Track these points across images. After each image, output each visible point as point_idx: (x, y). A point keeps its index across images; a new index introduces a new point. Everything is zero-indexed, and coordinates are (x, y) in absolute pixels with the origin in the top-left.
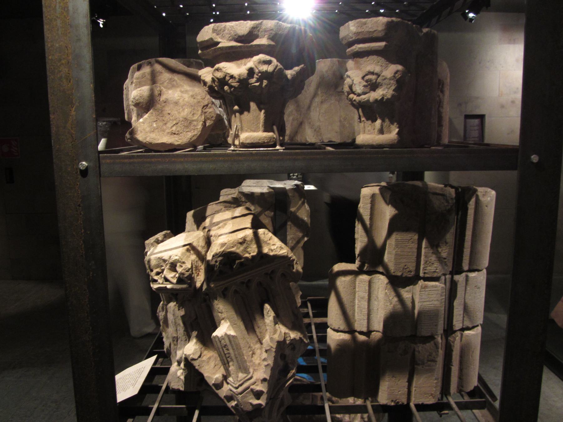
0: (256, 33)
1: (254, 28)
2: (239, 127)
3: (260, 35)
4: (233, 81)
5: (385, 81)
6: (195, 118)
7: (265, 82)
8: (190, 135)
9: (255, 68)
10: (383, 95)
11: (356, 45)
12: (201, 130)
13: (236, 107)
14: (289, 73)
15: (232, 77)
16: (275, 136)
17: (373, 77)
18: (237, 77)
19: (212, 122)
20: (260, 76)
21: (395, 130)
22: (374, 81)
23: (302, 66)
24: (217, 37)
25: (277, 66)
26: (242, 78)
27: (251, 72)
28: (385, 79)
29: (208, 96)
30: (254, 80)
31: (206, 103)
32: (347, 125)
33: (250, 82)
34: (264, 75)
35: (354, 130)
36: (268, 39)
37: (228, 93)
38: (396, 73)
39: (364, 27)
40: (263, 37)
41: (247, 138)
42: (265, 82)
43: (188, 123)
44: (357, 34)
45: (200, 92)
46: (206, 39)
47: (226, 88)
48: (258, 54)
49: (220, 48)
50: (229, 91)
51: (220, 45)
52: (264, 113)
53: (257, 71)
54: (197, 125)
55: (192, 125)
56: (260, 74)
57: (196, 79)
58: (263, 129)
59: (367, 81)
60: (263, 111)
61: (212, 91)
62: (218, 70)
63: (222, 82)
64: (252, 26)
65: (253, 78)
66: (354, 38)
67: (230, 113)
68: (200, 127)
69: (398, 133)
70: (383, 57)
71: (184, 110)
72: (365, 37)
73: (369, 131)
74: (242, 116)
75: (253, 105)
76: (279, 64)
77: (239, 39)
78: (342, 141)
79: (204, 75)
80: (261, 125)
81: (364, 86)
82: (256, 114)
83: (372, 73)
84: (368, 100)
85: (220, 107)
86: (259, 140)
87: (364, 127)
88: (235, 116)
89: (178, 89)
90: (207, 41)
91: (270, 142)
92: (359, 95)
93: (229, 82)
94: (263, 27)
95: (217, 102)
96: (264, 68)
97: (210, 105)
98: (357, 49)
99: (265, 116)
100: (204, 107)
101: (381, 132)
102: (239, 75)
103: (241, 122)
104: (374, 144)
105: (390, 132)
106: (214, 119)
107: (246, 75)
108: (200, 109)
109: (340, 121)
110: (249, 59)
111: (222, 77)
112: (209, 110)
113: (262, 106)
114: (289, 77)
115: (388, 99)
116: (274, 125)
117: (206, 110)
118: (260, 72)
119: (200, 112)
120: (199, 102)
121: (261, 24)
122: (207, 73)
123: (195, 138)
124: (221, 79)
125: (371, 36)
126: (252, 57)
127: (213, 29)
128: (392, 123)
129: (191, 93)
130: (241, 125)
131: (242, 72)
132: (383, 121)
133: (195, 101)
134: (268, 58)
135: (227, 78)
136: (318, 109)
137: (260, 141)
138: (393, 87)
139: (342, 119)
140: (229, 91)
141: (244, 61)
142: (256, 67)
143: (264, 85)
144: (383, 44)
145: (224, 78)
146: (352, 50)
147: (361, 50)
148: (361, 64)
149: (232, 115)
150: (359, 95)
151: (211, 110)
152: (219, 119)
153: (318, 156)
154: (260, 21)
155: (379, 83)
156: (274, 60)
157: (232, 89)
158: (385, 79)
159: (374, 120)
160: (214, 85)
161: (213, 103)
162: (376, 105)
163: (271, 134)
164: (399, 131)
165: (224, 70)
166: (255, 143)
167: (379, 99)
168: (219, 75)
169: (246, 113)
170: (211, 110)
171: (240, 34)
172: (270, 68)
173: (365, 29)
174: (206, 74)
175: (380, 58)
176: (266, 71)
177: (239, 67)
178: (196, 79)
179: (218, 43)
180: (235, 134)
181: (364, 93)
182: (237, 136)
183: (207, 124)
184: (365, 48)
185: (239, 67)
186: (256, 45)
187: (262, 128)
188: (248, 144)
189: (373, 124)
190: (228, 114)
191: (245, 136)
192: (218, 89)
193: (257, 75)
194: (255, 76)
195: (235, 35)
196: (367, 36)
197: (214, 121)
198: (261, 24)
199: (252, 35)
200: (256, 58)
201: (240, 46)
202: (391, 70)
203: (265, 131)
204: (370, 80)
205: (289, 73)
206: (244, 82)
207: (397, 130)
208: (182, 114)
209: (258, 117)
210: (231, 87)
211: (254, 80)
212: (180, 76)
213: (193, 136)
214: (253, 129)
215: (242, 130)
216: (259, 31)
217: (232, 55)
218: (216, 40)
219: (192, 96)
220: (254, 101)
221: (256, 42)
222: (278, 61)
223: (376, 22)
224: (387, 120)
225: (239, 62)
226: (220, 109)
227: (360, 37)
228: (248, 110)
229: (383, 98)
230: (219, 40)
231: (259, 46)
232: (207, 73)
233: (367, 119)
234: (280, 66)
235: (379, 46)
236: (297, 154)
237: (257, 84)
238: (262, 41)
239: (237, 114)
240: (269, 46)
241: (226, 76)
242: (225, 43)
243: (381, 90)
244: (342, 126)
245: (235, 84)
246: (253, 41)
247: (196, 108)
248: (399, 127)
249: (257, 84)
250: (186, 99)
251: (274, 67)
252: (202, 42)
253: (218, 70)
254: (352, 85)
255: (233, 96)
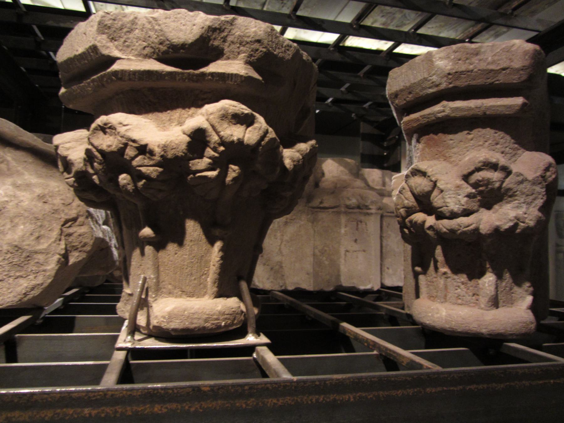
0: (216, 43)
1: (212, 30)
2: (151, 283)
3: (226, 50)
4: (146, 162)
5: (522, 186)
6: (43, 245)
7: (233, 171)
8: (24, 285)
9: (210, 129)
10: (517, 218)
11: (444, 103)
12: (53, 273)
13: (147, 231)
14: (290, 156)
15: (143, 150)
16: (243, 308)
17: (495, 176)
18: (157, 150)
19: (84, 255)
20: (221, 153)
21: (523, 298)
22: (497, 185)
23: (313, 142)
24: (110, 44)
25: (266, 132)
26: (170, 155)
27: (198, 139)
28: (521, 182)
29: (77, 202)
30: (205, 162)
31: (73, 213)
32: (327, 263)
33: (194, 168)
34: (234, 151)
35: (339, 271)
36: (248, 63)
37: (127, 192)
38: (547, 169)
39: (475, 60)
40: (235, 56)
41: (171, 316)
42: (233, 171)
43: (21, 257)
44: (457, 75)
45: (59, 188)
46: (81, 50)
47: (124, 178)
48: (217, 101)
49: (116, 73)
50: (130, 187)
51: (116, 67)
52: (222, 250)
53: (215, 138)
54: (46, 262)
55: (32, 262)
56: (222, 148)
57: (51, 160)
58: (215, 289)
59: (475, 185)
60: (218, 245)
61: (84, 186)
62: (103, 129)
63: (115, 161)
64: (208, 23)
65: (201, 156)
66: (443, 86)
67: (131, 243)
68: (52, 266)
69: (533, 308)
70: (507, 132)
71: (15, 226)
72: (473, 83)
73: (458, 297)
74: (161, 254)
75: (193, 229)
76: (270, 129)
77: (171, 53)
78: (317, 289)
79: (67, 145)
80: (209, 280)
81: (469, 196)
82: (200, 252)
83: (494, 167)
84: (477, 230)
85: (105, 223)
86: (206, 321)
87: (446, 287)
88: (143, 254)
89: (9, 181)
90: (82, 56)
91: (232, 324)
92: (453, 216)
93: (134, 163)
94: (237, 32)
95: (100, 214)
96: (236, 132)
97: (81, 219)
98: (448, 112)
99: (222, 258)
100: (67, 222)
101: (495, 303)
102: (165, 148)
103: (157, 269)
104: (484, 331)
105: (511, 302)
106: (88, 248)
107: (184, 147)
108: (57, 227)
109: (314, 255)
110: (193, 110)
111: (114, 148)
112: (77, 230)
113: (217, 232)
114: (288, 163)
115: (528, 228)
116: (240, 278)
117: (71, 230)
118: (223, 143)
119: (55, 234)
120: (56, 211)
121: (231, 23)
122: (77, 141)
123: (36, 292)
124: (112, 152)
125: (489, 81)
126: (200, 106)
127: (100, 23)
128: (518, 282)
129: (38, 191)
130: (158, 278)
131: (173, 138)
132: (500, 277)
133: (47, 207)
134: (244, 109)
135: (130, 152)
136: (279, 234)
137: (208, 325)
138: (540, 202)
139: (317, 251)
140: (130, 187)
141: (177, 113)
142: (213, 127)
143: (229, 179)
144: (519, 101)
145: (122, 151)
146: (423, 117)
147: (458, 114)
148: (449, 147)
149: (133, 249)
150: (453, 216)
151: (83, 230)
152: (100, 248)
153: (400, 392)
154: (230, 17)
155: (509, 189)
156: (261, 121)
157: (141, 183)
158: (521, 182)
159: (475, 273)
160: (91, 171)
161: (90, 215)
162: (489, 240)
163: (232, 303)
164: (534, 301)
165: (122, 130)
166: (192, 330)
167: (506, 227)
168: (107, 142)
169: (172, 247)
170: (83, 230)
171: (175, 41)
172: (250, 135)
173: (476, 64)
174: (72, 144)
175: (501, 134)
176: (240, 142)
177: (163, 126)
178: (51, 160)
179: (112, 60)
180: (140, 298)
181: (467, 213)
182: (143, 304)
183: (72, 260)
184: (470, 109)
185: (164, 128)
186: (212, 74)
187: (212, 288)
188: (175, 330)
189: (473, 282)
190: (121, 245)
191: (167, 309)
192: (99, 183)
193: (215, 149)
194: (209, 152)
195: (161, 44)
196: (479, 81)
197: (88, 252)
198: (231, 23)
199: (205, 49)
200: (210, 108)
201: (170, 74)
202: (531, 164)
203: (220, 294)
204: (488, 182)
205: (290, 156)
206: (174, 166)
207: (529, 299)
208: (9, 237)
209: (203, 260)
210: (137, 175)
211: (205, 162)
212: (19, 154)
213: (33, 289)
214: (188, 289)
215: (158, 289)
216: (224, 40)
217: (148, 96)
218: (105, 52)
219: (41, 198)
220: (196, 217)
221: (214, 68)
222: (268, 122)
223: (508, 50)
224: (507, 275)
225: (164, 116)
226: (105, 227)
227: (462, 83)
228: (179, 238)
229: (516, 225)
230: (116, 53)
231: (223, 77)
232: (77, 141)
233: (456, 271)
234: (272, 134)
235: (509, 107)
236: (339, 387)
237: (212, 174)
238: (234, 66)
239: (149, 249)
240: (248, 79)
241: (126, 145)
242: (129, 62)
243: (509, 206)
244: (318, 263)
245: (152, 171)
246: (206, 63)
247: (46, 223)
248: (534, 294)
249: (212, 174)
250: (25, 204)
251: (261, 132)
252: (70, 61)
253: (103, 129)
254: (429, 193)
255: (146, 203)
